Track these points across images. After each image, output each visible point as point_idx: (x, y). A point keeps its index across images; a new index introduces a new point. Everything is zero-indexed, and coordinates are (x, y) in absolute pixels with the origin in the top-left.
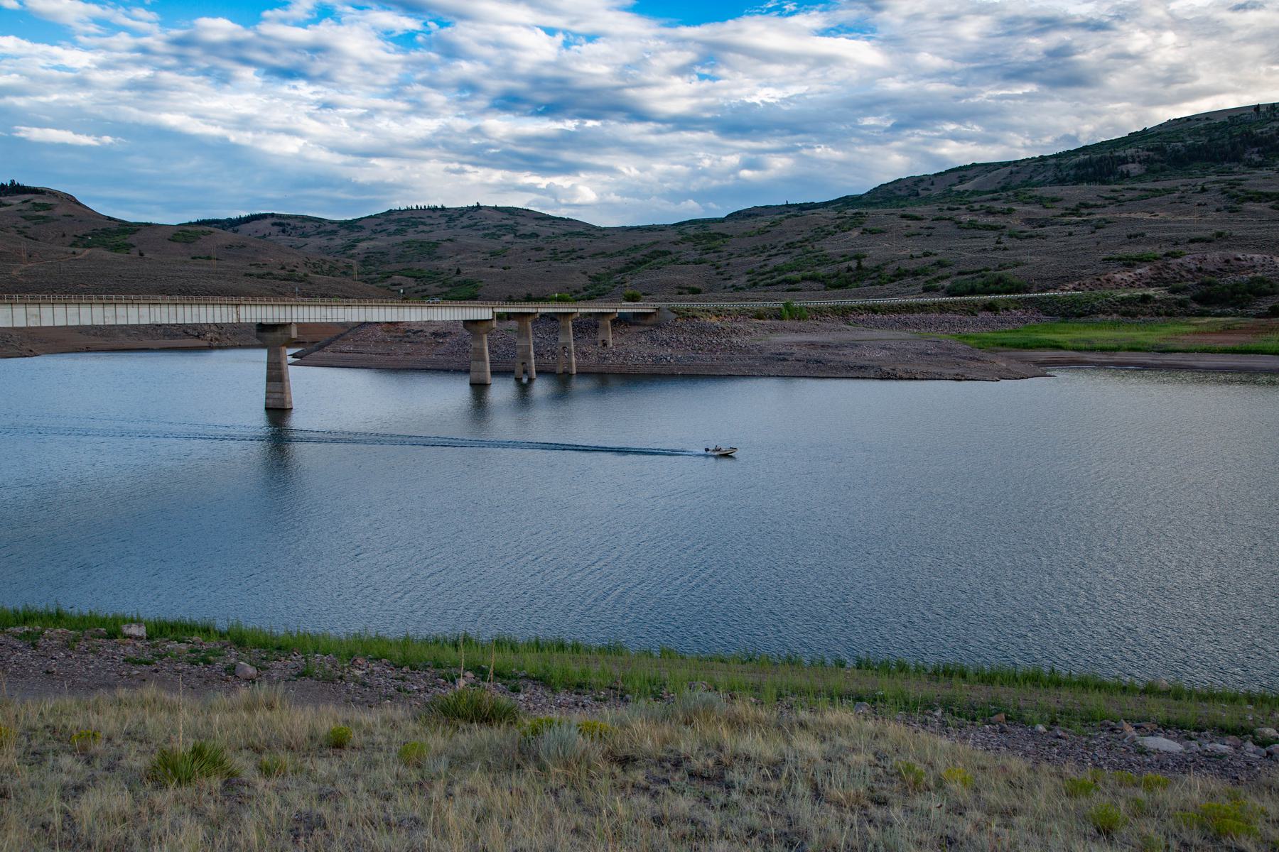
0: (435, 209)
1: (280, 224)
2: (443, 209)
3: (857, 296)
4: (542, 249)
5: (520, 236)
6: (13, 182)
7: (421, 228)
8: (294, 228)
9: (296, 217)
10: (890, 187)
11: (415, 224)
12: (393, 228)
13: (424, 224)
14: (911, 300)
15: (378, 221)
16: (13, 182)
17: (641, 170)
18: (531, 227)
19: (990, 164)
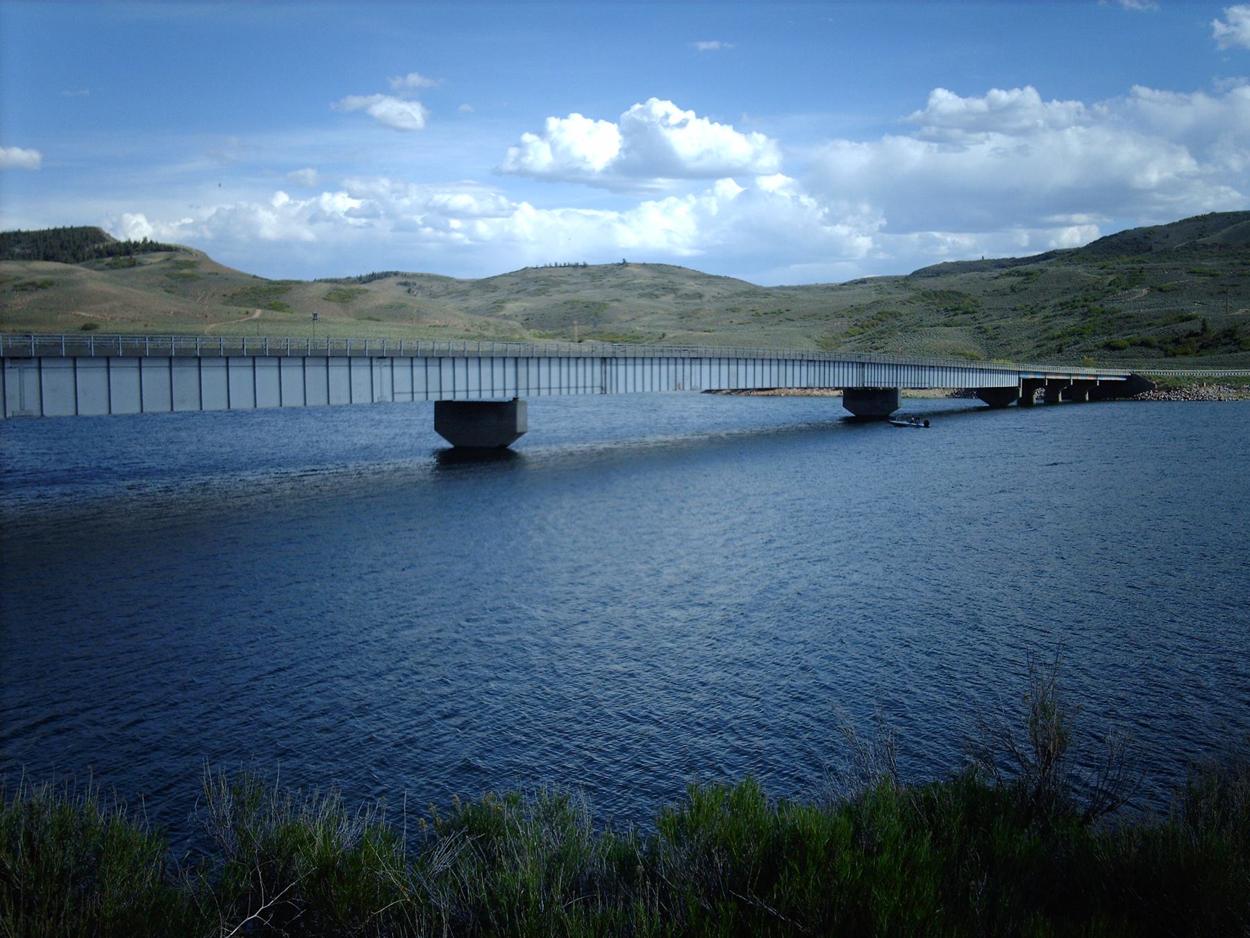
0: (576, 266)
1: (405, 284)
2: (585, 266)
3: (38, 272)
4: (739, 310)
5: (681, 297)
6: (145, 239)
7: (565, 287)
8: (420, 288)
9: (422, 275)
10: (1114, 240)
11: (557, 284)
12: (532, 288)
13: (565, 282)
14: (1087, 372)
15: (514, 280)
16: (145, 239)
17: (1199, 142)
18: (691, 286)
19: (1235, 214)
